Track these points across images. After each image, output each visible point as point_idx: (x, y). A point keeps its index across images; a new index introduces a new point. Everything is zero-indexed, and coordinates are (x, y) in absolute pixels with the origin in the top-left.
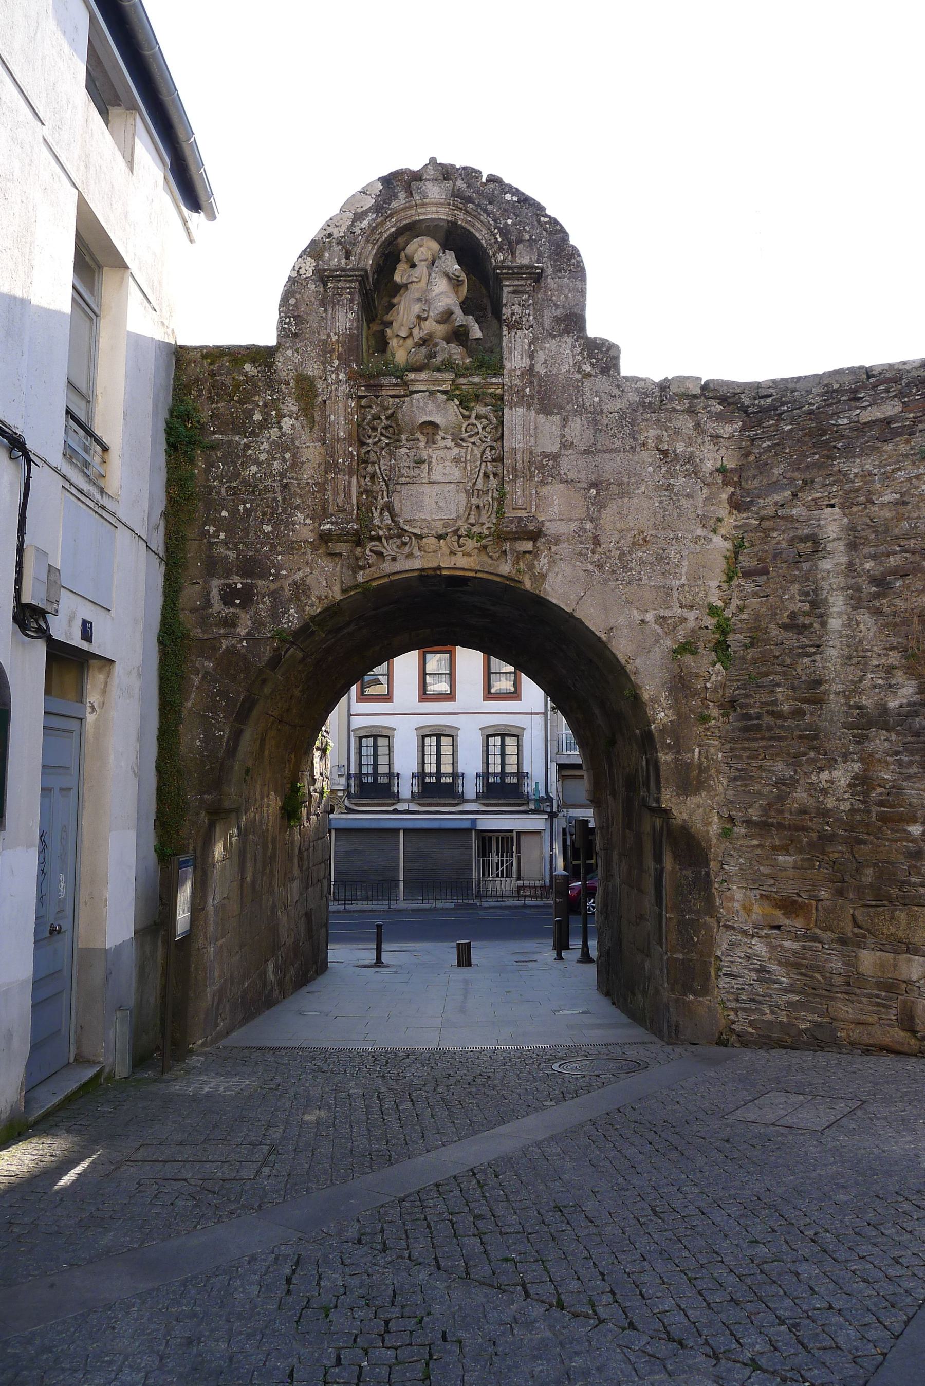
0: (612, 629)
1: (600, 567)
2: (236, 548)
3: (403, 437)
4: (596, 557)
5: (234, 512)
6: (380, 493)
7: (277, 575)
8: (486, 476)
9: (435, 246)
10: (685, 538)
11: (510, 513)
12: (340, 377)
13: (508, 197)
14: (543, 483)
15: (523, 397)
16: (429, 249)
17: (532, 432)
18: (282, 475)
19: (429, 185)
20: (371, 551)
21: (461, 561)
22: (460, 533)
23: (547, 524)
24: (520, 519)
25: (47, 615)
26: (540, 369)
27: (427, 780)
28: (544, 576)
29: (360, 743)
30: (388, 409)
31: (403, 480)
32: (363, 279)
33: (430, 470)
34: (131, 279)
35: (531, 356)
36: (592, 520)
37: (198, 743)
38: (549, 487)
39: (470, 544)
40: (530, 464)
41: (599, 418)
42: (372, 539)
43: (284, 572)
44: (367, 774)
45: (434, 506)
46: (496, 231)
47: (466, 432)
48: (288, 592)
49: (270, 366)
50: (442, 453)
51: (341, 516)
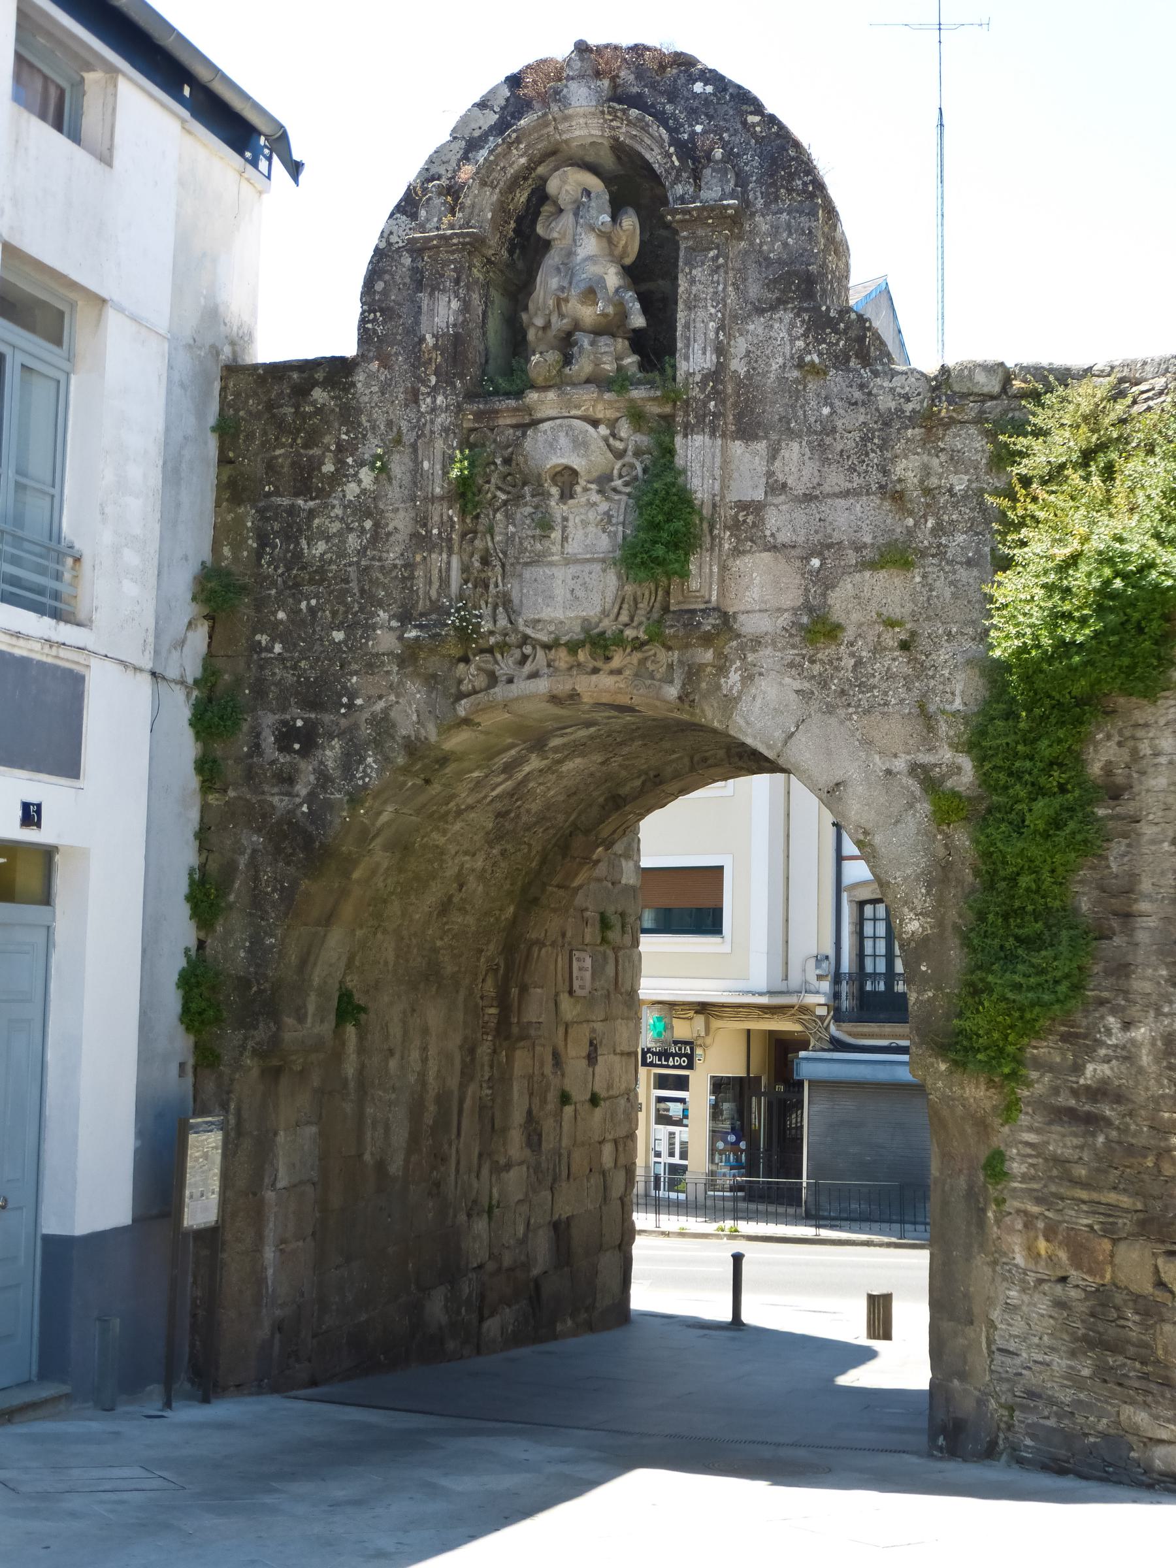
0: (838, 784)
1: (824, 684)
2: (295, 667)
4: (817, 669)
5: (294, 612)
7: (350, 706)
10: (963, 634)
12: (438, 402)
13: (698, 87)
14: (737, 552)
15: (705, 416)
17: (717, 473)
18: (361, 553)
19: (573, 85)
20: (479, 669)
23: (742, 618)
33: (565, 539)
37: (242, 955)
38: (747, 559)
43: (359, 702)
45: (569, 595)
48: (366, 731)
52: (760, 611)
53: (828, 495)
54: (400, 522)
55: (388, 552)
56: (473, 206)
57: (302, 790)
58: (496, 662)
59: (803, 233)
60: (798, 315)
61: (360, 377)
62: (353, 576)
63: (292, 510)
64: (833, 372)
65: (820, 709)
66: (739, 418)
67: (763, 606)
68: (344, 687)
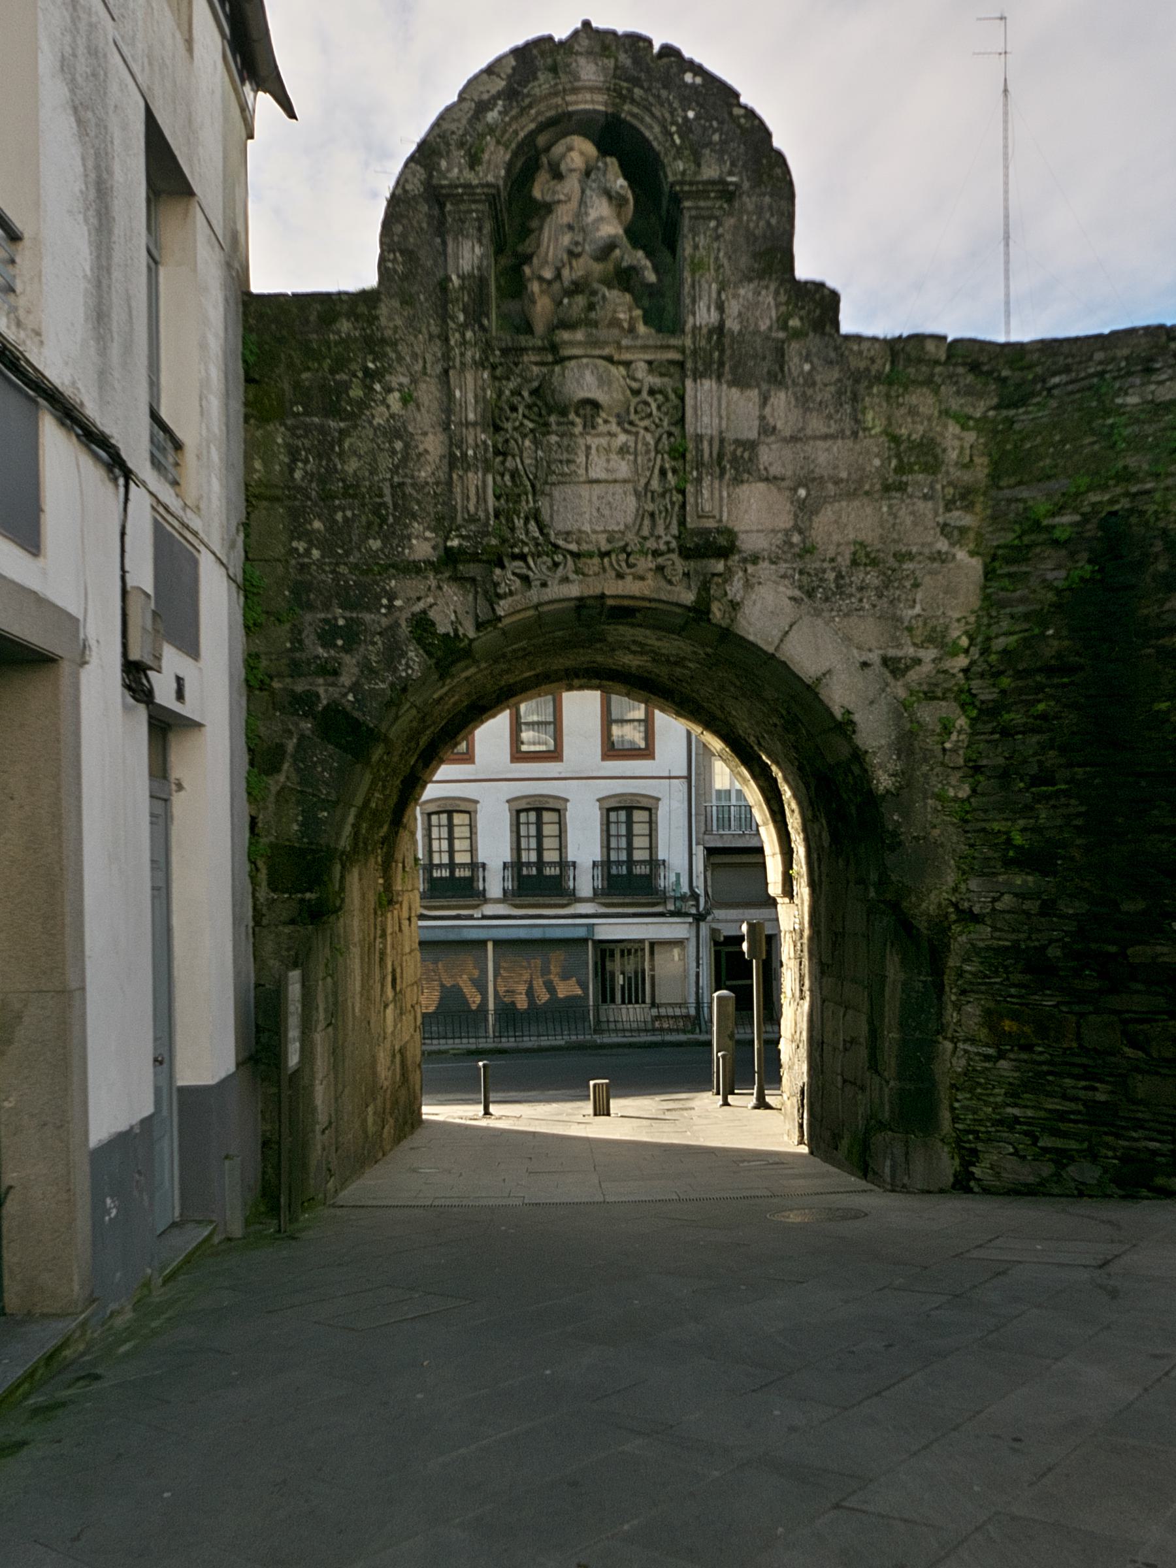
1: (810, 594)
3: (553, 419)
6: (523, 498)
7: (390, 607)
8: (663, 473)
9: (590, 149)
11: (691, 523)
13: (688, 78)
16: (582, 153)
18: (395, 470)
19: (582, 61)
21: (632, 587)
22: (629, 549)
23: (742, 536)
24: (708, 531)
25: (150, 673)
26: (733, 325)
27: (525, 871)
28: (735, 606)
29: (429, 820)
30: (530, 381)
31: (553, 478)
32: (493, 201)
34: (198, 209)
35: (721, 308)
36: (800, 532)
38: (745, 487)
39: (645, 564)
40: (721, 456)
41: (809, 392)
42: (514, 557)
44: (440, 866)
45: (595, 514)
46: (674, 129)
47: (636, 412)
49: (373, 319)
50: (603, 441)
51: (473, 527)
52: (758, 531)
53: (809, 438)
54: (433, 445)
55: (419, 470)
56: (489, 162)
57: (346, 680)
58: (529, 568)
59: (783, 214)
60: (781, 284)
61: (383, 310)
62: (387, 491)
63: (323, 430)
64: (811, 335)
65: (809, 613)
66: (734, 370)
67: (760, 527)
68: (384, 589)
